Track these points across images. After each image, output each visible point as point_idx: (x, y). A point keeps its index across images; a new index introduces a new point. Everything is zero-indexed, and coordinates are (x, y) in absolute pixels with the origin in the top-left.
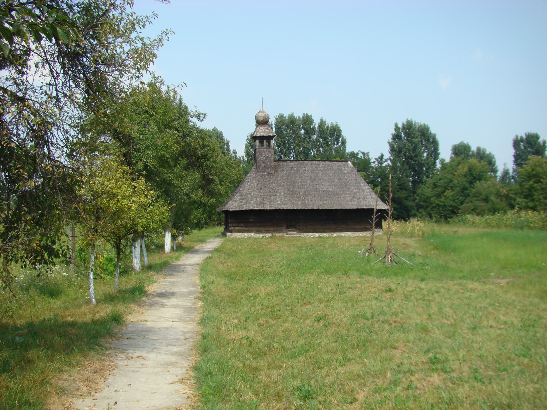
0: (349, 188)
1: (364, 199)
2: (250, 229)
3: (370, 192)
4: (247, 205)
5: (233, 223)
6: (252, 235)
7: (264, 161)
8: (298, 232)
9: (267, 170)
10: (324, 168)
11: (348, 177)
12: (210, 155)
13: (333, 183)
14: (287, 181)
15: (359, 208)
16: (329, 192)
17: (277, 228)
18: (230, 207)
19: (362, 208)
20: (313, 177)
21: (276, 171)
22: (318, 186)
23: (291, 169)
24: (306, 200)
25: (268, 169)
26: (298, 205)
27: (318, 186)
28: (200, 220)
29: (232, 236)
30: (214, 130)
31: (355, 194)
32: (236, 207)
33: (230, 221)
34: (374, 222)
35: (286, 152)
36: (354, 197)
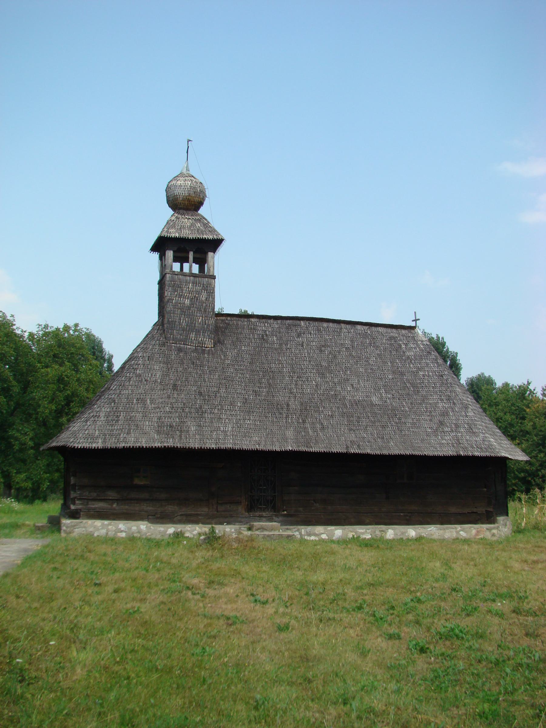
5: (82, 487)
7: (185, 310)
8: (284, 523)
9: (193, 335)
10: (352, 341)
17: (221, 508)
18: (76, 437)
20: (324, 364)
26: (285, 439)
31: (445, 414)
32: (94, 438)
36: (441, 423)
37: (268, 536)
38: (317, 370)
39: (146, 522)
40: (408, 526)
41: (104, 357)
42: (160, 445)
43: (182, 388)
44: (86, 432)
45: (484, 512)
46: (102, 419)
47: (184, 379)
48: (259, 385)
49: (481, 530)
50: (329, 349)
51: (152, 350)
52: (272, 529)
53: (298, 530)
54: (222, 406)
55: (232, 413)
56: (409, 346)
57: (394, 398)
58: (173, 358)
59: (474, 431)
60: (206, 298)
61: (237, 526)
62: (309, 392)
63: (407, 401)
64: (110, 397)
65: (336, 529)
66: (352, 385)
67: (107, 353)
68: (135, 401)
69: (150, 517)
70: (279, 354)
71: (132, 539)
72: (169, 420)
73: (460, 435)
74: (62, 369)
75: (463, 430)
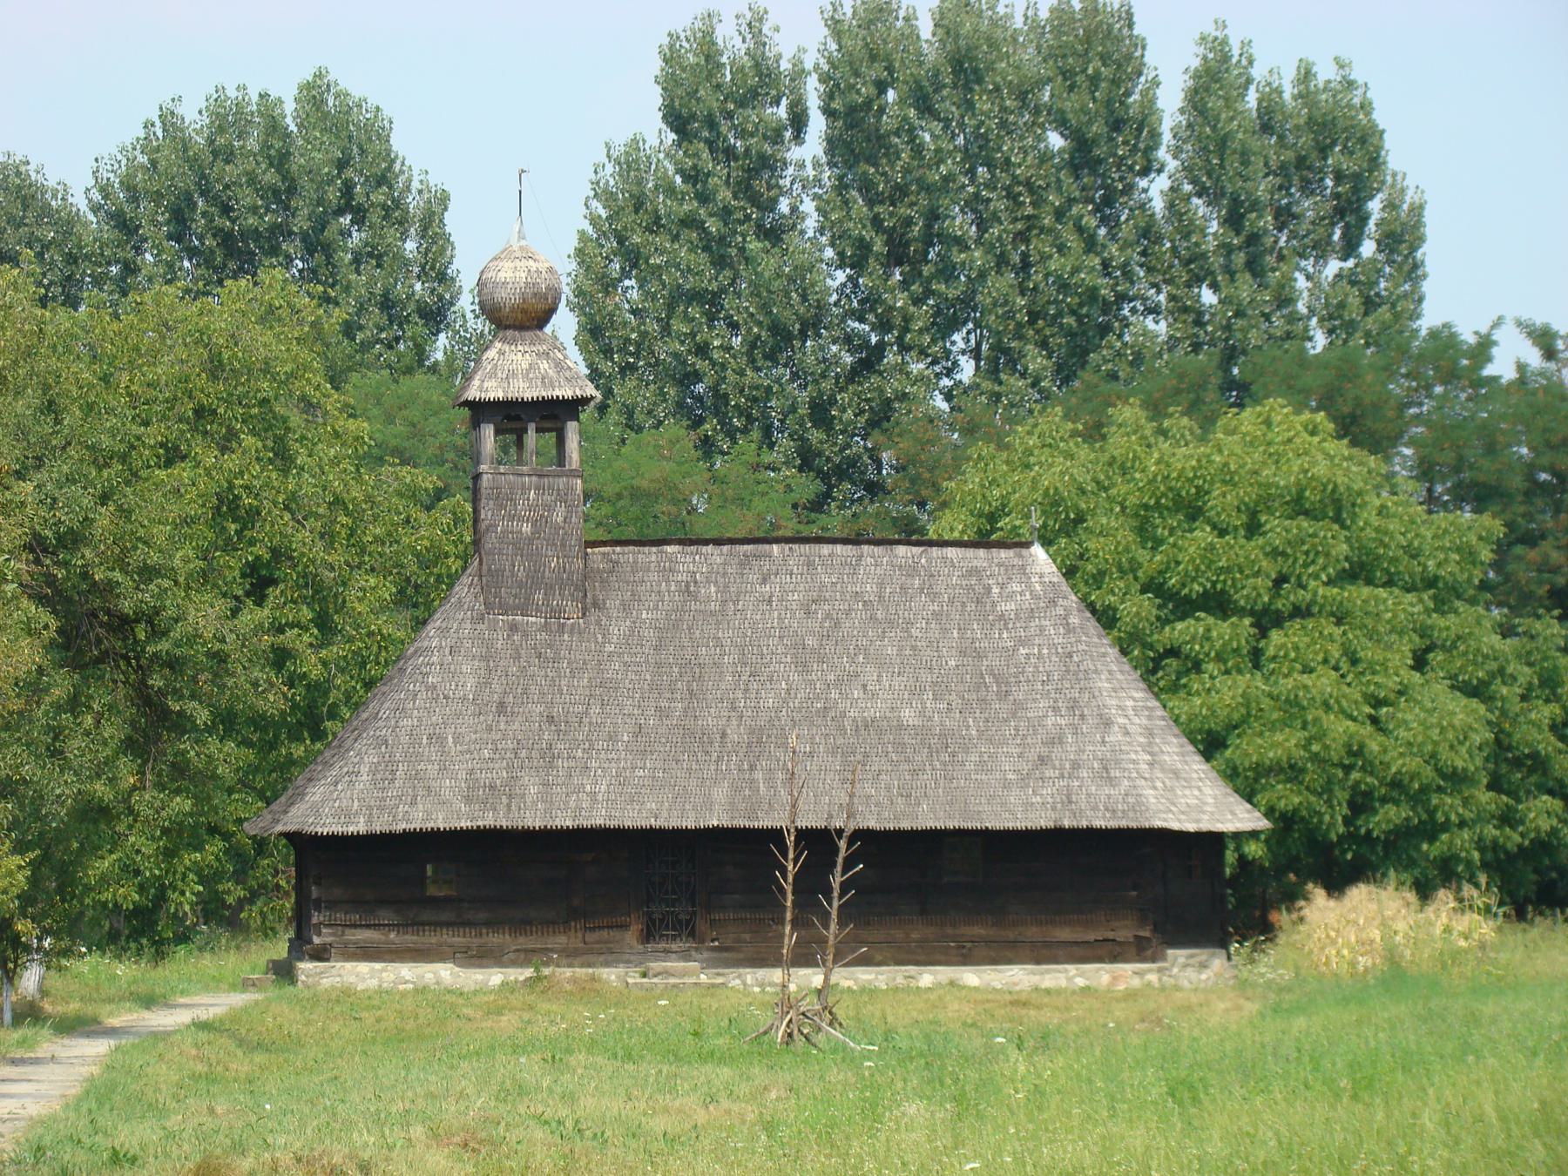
0: (1018, 706)
1: (1105, 774)
2: (431, 939)
3: (1150, 733)
4: (413, 803)
5: (332, 905)
6: (444, 973)
7: (521, 546)
8: (709, 964)
9: (539, 597)
10: (881, 585)
11: (1022, 642)
12: (171, 612)
13: (927, 677)
14: (658, 665)
15: (1067, 823)
16: (901, 727)
17: (591, 937)
18: (318, 815)
19: (1084, 824)
20: (811, 642)
21: (595, 605)
22: (834, 694)
23: (687, 591)
24: (759, 775)
25: (549, 589)
26: (709, 805)
27: (834, 694)
28: (162, 889)
29: (326, 982)
30: (314, 94)
31: (1056, 740)
32: (349, 815)
33: (315, 892)
34: (836, 904)
35: (907, 319)
36: (1042, 760)
37: (674, 986)
38: (795, 656)
39: (451, 965)
40: (963, 968)
41: (397, 203)
42: (469, 824)
43: (516, 710)
44: (336, 805)
45: (1131, 940)
46: (365, 777)
47: (519, 691)
48: (669, 695)
49: (1121, 976)
50: (826, 607)
51: (456, 632)
52: (684, 974)
53: (739, 976)
54: (592, 748)
55: (610, 757)
56: (1010, 589)
57: (949, 710)
58: (499, 646)
59: (1112, 775)
60: (565, 518)
61: (621, 970)
62: (770, 705)
63: (977, 715)
64: (378, 733)
65: (815, 974)
66: (864, 686)
67: (415, 185)
68: (425, 741)
69: (458, 955)
70: (718, 623)
71: (421, 990)
72: (489, 775)
73: (1076, 784)
74: (232, 462)
75: (1085, 775)
